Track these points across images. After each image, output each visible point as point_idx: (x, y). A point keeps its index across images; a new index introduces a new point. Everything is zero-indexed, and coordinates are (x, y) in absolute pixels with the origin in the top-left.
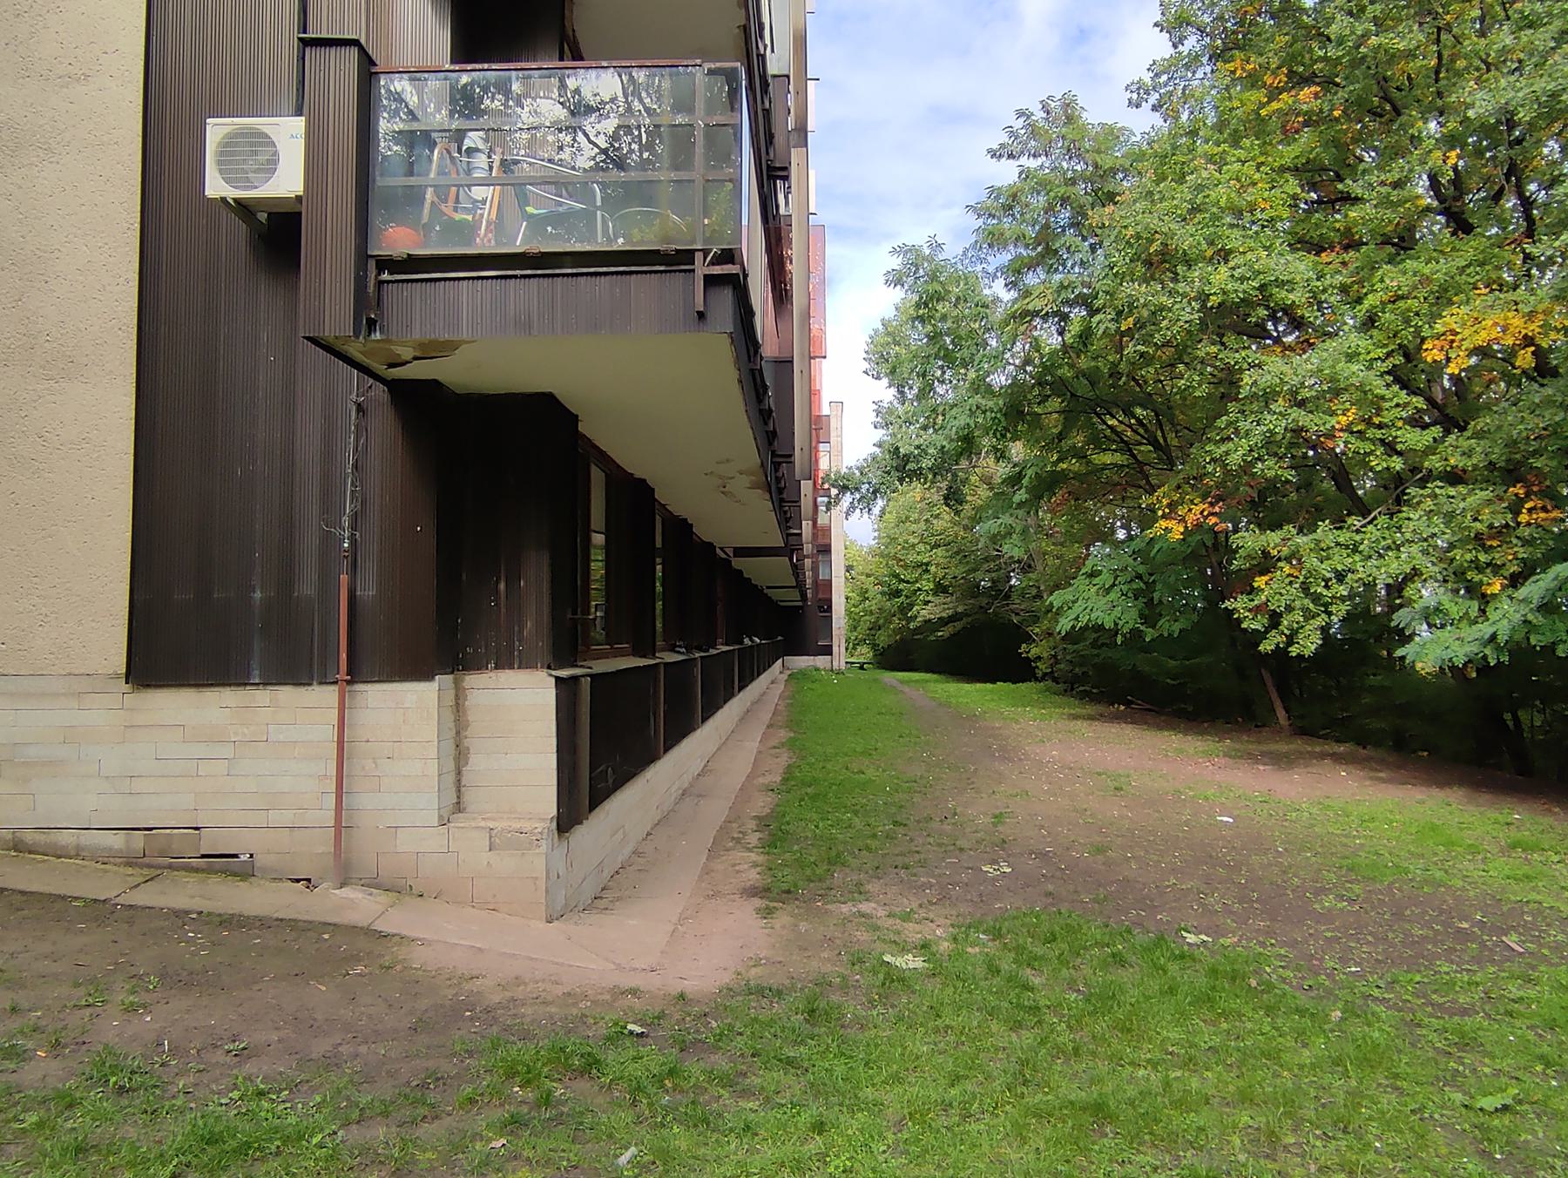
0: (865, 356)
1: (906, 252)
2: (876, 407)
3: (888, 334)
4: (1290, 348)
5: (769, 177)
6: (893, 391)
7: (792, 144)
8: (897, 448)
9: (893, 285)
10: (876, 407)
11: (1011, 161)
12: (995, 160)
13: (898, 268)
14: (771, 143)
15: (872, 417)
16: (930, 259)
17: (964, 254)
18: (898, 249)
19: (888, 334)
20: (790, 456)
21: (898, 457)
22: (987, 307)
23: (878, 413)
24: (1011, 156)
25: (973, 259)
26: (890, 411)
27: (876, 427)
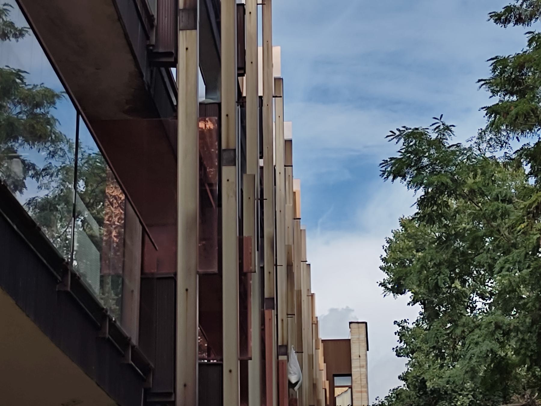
0: (382, 264)
1: (408, 136)
2: (398, 329)
3: (409, 237)
4: (388, 289)
5: (151, 64)
6: (418, 308)
7: (180, 25)
8: (424, 382)
9: (391, 177)
10: (398, 329)
11: (520, 26)
12: (499, 25)
13: (398, 155)
14: (152, 26)
15: (395, 342)
16: (439, 143)
17: (480, 137)
18: (398, 133)
19: (409, 237)
20: (169, 395)
21: (425, 393)
22: (510, 202)
23: (402, 335)
24: (519, 20)
25: (492, 143)
26: (414, 334)
27: (398, 355)
